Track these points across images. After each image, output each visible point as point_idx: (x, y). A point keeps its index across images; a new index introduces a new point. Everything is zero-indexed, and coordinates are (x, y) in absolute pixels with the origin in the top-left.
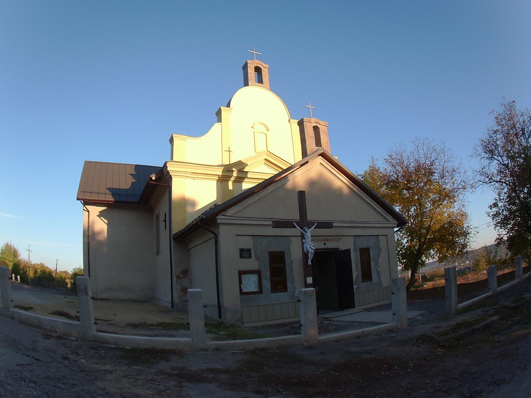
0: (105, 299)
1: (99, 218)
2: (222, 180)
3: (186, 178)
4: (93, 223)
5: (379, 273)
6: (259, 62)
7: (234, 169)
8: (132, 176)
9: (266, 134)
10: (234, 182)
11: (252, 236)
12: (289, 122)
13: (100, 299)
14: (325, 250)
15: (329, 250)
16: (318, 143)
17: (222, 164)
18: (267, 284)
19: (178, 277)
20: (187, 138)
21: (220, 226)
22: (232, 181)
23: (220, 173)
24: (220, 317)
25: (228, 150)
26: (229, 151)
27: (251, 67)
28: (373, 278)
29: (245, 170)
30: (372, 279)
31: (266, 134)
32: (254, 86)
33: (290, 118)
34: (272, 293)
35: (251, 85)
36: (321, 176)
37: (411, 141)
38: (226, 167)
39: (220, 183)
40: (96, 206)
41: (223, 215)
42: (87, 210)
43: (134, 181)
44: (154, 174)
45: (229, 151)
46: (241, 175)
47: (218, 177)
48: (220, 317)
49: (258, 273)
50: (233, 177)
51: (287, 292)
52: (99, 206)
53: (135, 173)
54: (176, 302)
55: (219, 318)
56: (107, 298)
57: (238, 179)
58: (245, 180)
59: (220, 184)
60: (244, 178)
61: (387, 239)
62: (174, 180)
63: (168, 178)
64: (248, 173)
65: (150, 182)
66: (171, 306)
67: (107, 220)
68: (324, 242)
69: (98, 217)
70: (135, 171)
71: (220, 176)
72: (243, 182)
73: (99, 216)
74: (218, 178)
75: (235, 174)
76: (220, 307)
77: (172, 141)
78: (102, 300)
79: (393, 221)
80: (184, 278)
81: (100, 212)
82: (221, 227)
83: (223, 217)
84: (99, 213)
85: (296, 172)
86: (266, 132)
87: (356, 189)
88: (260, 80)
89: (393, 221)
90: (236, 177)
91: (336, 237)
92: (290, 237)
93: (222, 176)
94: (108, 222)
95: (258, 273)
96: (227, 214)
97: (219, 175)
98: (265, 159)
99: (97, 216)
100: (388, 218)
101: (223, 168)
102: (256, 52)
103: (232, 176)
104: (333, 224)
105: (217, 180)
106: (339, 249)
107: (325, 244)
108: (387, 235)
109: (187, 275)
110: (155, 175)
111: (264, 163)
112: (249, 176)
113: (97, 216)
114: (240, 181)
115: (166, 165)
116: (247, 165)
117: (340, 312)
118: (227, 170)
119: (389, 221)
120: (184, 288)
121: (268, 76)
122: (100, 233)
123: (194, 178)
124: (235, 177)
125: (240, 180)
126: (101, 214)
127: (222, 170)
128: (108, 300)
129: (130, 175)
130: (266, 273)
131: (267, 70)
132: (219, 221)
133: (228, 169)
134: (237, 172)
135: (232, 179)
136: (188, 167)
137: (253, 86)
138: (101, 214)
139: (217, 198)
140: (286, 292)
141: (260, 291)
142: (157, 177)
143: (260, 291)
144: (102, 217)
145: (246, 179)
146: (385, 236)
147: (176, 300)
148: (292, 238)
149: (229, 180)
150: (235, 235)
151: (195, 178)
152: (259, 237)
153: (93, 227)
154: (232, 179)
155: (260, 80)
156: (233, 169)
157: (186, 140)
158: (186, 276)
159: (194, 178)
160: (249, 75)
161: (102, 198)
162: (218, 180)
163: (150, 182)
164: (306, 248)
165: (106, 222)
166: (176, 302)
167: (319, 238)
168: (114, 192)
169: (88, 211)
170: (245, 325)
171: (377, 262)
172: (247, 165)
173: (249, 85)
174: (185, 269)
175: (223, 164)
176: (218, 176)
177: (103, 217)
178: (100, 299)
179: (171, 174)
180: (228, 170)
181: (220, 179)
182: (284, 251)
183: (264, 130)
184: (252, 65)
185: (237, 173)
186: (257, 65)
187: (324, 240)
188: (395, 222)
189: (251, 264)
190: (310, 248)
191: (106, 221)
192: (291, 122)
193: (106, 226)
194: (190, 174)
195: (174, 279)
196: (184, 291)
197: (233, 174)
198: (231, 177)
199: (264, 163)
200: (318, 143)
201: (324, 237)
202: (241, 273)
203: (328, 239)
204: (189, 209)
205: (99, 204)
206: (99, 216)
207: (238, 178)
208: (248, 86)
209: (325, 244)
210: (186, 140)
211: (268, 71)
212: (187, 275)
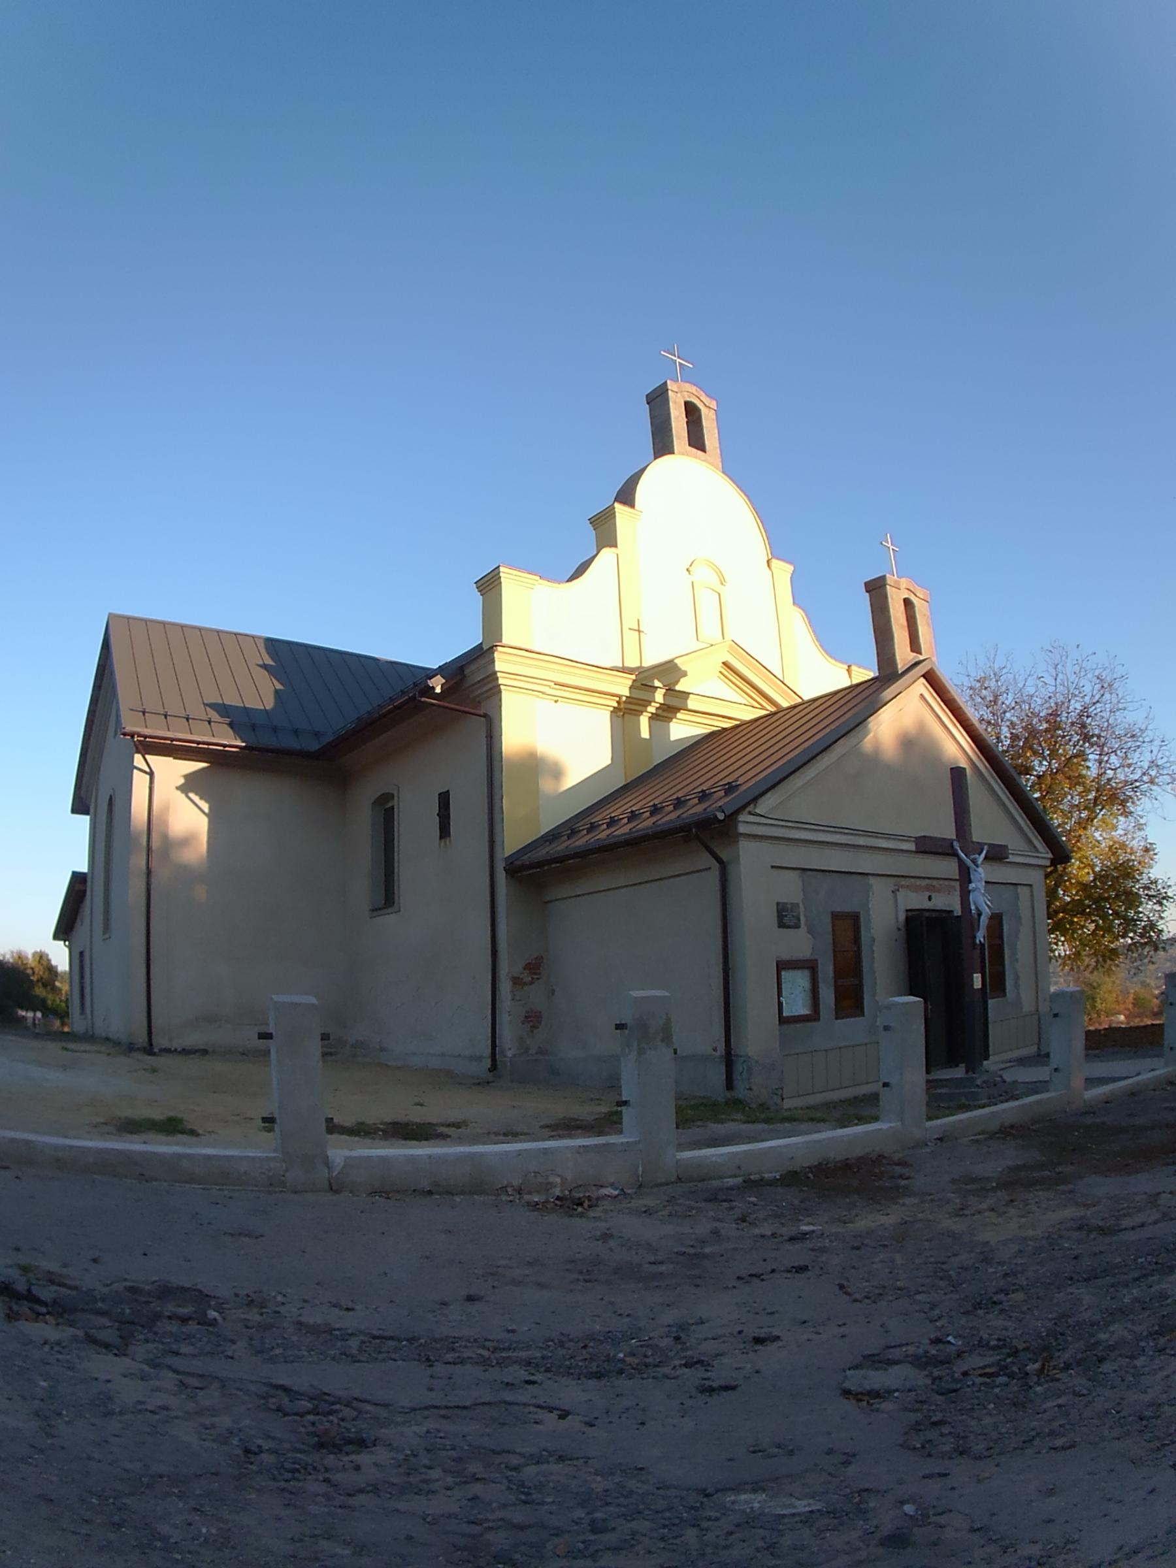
0: (195, 1052)
1: (183, 796)
2: (626, 709)
3: (538, 697)
4: (166, 809)
5: (1017, 977)
6: (694, 389)
7: (657, 683)
8: (266, 669)
9: (719, 594)
10: (654, 717)
11: (798, 872)
12: (769, 566)
13: (179, 1049)
14: (937, 914)
15: (914, 913)
16: (915, 646)
17: (621, 666)
18: (828, 996)
19: (517, 981)
20: (535, 582)
21: (740, 842)
22: (650, 715)
23: (625, 692)
24: (730, 1085)
25: (637, 628)
26: (639, 631)
27: (677, 400)
28: (1007, 991)
29: (678, 688)
30: (1004, 990)
31: (719, 594)
32: (687, 455)
33: (770, 557)
34: (837, 1018)
35: (679, 453)
36: (921, 726)
37: (1042, 648)
38: (642, 676)
39: (618, 716)
40: (175, 758)
41: (750, 813)
42: (148, 770)
43: (279, 687)
44: (442, 677)
45: (639, 631)
46: (673, 702)
47: (618, 702)
48: (730, 1085)
49: (810, 966)
50: (653, 704)
51: (863, 1015)
52: (183, 757)
53: (272, 663)
54: (510, 1054)
55: (728, 1089)
56: (202, 1047)
57: (664, 710)
58: (679, 715)
59: (620, 720)
60: (679, 710)
61: (1032, 895)
62: (505, 696)
63: (479, 692)
64: (688, 697)
65: (423, 699)
66: (489, 1066)
67: (206, 801)
68: (928, 894)
69: (179, 792)
70: (272, 659)
71: (624, 699)
72: (674, 720)
73: (184, 789)
74: (616, 705)
75: (659, 697)
76: (729, 1060)
77: (489, 585)
78: (185, 1052)
79: (1044, 851)
80: (532, 983)
81: (186, 777)
82: (744, 846)
83: (752, 818)
84: (182, 781)
85: (884, 711)
86: (719, 588)
87: (982, 765)
88: (696, 441)
89: (1044, 851)
90: (661, 704)
91: (947, 883)
92: (870, 877)
93: (630, 700)
94: (210, 808)
95: (810, 966)
96: (758, 811)
97: (620, 696)
98: (723, 663)
99: (178, 788)
100: (1036, 842)
101: (633, 677)
102: (672, 359)
103: (650, 702)
104: (913, 848)
105: (612, 709)
106: (952, 911)
107: (930, 898)
108: (1031, 886)
109: (539, 974)
110: (444, 681)
111: (720, 672)
112: (692, 703)
113: (178, 788)
114: (666, 717)
115: (493, 653)
116: (684, 674)
117: (952, 1069)
118: (642, 685)
119: (1037, 851)
120: (530, 1014)
121: (716, 431)
122: (186, 841)
123: (556, 698)
124: (658, 705)
125: (667, 712)
126: (190, 784)
127: (630, 683)
128: (204, 1052)
129: (259, 668)
130: (827, 970)
131: (712, 415)
132: (742, 829)
133: (643, 680)
134: (664, 691)
135: (651, 709)
136: (548, 665)
137: (683, 454)
138: (190, 784)
139: (612, 759)
140: (859, 1016)
141: (814, 1016)
142: (445, 687)
143: (814, 1016)
144: (192, 791)
145: (682, 711)
146: (1028, 888)
147: (510, 1049)
148: (872, 880)
149: (641, 712)
150: (769, 866)
151: (560, 699)
152: (815, 873)
153: (165, 823)
154: (651, 709)
155: (696, 441)
156: (653, 683)
157: (531, 586)
158: (538, 979)
159: (556, 698)
160: (673, 424)
161: (200, 736)
162: (615, 711)
163: (423, 699)
164: (975, 904)
165: (207, 810)
166: (510, 1054)
167: (918, 882)
168: (238, 718)
169: (151, 774)
170: (787, 1104)
171: (1014, 953)
172: (684, 674)
173: (676, 451)
174: (536, 958)
175: (626, 665)
176: (618, 699)
177: (196, 794)
178: (180, 1052)
179: (501, 681)
180: (644, 683)
181: (622, 706)
182: (859, 913)
183: (714, 581)
184: (679, 395)
185: (664, 695)
186: (689, 397)
187: (928, 888)
188: (1047, 853)
189: (799, 944)
190: (986, 903)
191: (205, 807)
192: (773, 568)
193: (205, 820)
194: (550, 686)
195: (505, 987)
196: (531, 1021)
197: (654, 696)
198: (649, 703)
199: (720, 672)
200: (915, 646)
201: (927, 881)
202: (782, 966)
203: (934, 886)
204: (546, 785)
205: (193, 752)
206: (184, 789)
207: (665, 707)
208: (672, 452)
209: (930, 898)
210: (531, 586)
211: (714, 417)
212: (539, 974)
